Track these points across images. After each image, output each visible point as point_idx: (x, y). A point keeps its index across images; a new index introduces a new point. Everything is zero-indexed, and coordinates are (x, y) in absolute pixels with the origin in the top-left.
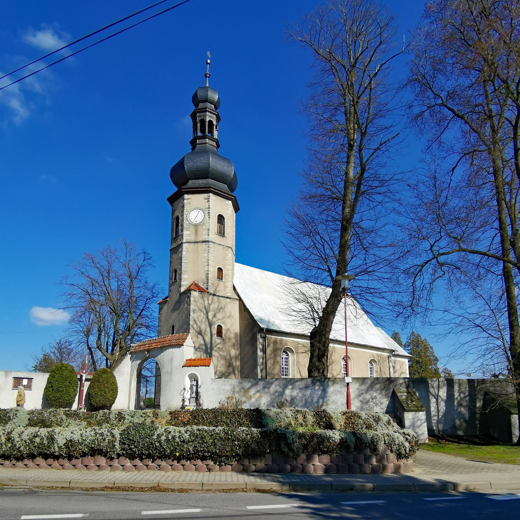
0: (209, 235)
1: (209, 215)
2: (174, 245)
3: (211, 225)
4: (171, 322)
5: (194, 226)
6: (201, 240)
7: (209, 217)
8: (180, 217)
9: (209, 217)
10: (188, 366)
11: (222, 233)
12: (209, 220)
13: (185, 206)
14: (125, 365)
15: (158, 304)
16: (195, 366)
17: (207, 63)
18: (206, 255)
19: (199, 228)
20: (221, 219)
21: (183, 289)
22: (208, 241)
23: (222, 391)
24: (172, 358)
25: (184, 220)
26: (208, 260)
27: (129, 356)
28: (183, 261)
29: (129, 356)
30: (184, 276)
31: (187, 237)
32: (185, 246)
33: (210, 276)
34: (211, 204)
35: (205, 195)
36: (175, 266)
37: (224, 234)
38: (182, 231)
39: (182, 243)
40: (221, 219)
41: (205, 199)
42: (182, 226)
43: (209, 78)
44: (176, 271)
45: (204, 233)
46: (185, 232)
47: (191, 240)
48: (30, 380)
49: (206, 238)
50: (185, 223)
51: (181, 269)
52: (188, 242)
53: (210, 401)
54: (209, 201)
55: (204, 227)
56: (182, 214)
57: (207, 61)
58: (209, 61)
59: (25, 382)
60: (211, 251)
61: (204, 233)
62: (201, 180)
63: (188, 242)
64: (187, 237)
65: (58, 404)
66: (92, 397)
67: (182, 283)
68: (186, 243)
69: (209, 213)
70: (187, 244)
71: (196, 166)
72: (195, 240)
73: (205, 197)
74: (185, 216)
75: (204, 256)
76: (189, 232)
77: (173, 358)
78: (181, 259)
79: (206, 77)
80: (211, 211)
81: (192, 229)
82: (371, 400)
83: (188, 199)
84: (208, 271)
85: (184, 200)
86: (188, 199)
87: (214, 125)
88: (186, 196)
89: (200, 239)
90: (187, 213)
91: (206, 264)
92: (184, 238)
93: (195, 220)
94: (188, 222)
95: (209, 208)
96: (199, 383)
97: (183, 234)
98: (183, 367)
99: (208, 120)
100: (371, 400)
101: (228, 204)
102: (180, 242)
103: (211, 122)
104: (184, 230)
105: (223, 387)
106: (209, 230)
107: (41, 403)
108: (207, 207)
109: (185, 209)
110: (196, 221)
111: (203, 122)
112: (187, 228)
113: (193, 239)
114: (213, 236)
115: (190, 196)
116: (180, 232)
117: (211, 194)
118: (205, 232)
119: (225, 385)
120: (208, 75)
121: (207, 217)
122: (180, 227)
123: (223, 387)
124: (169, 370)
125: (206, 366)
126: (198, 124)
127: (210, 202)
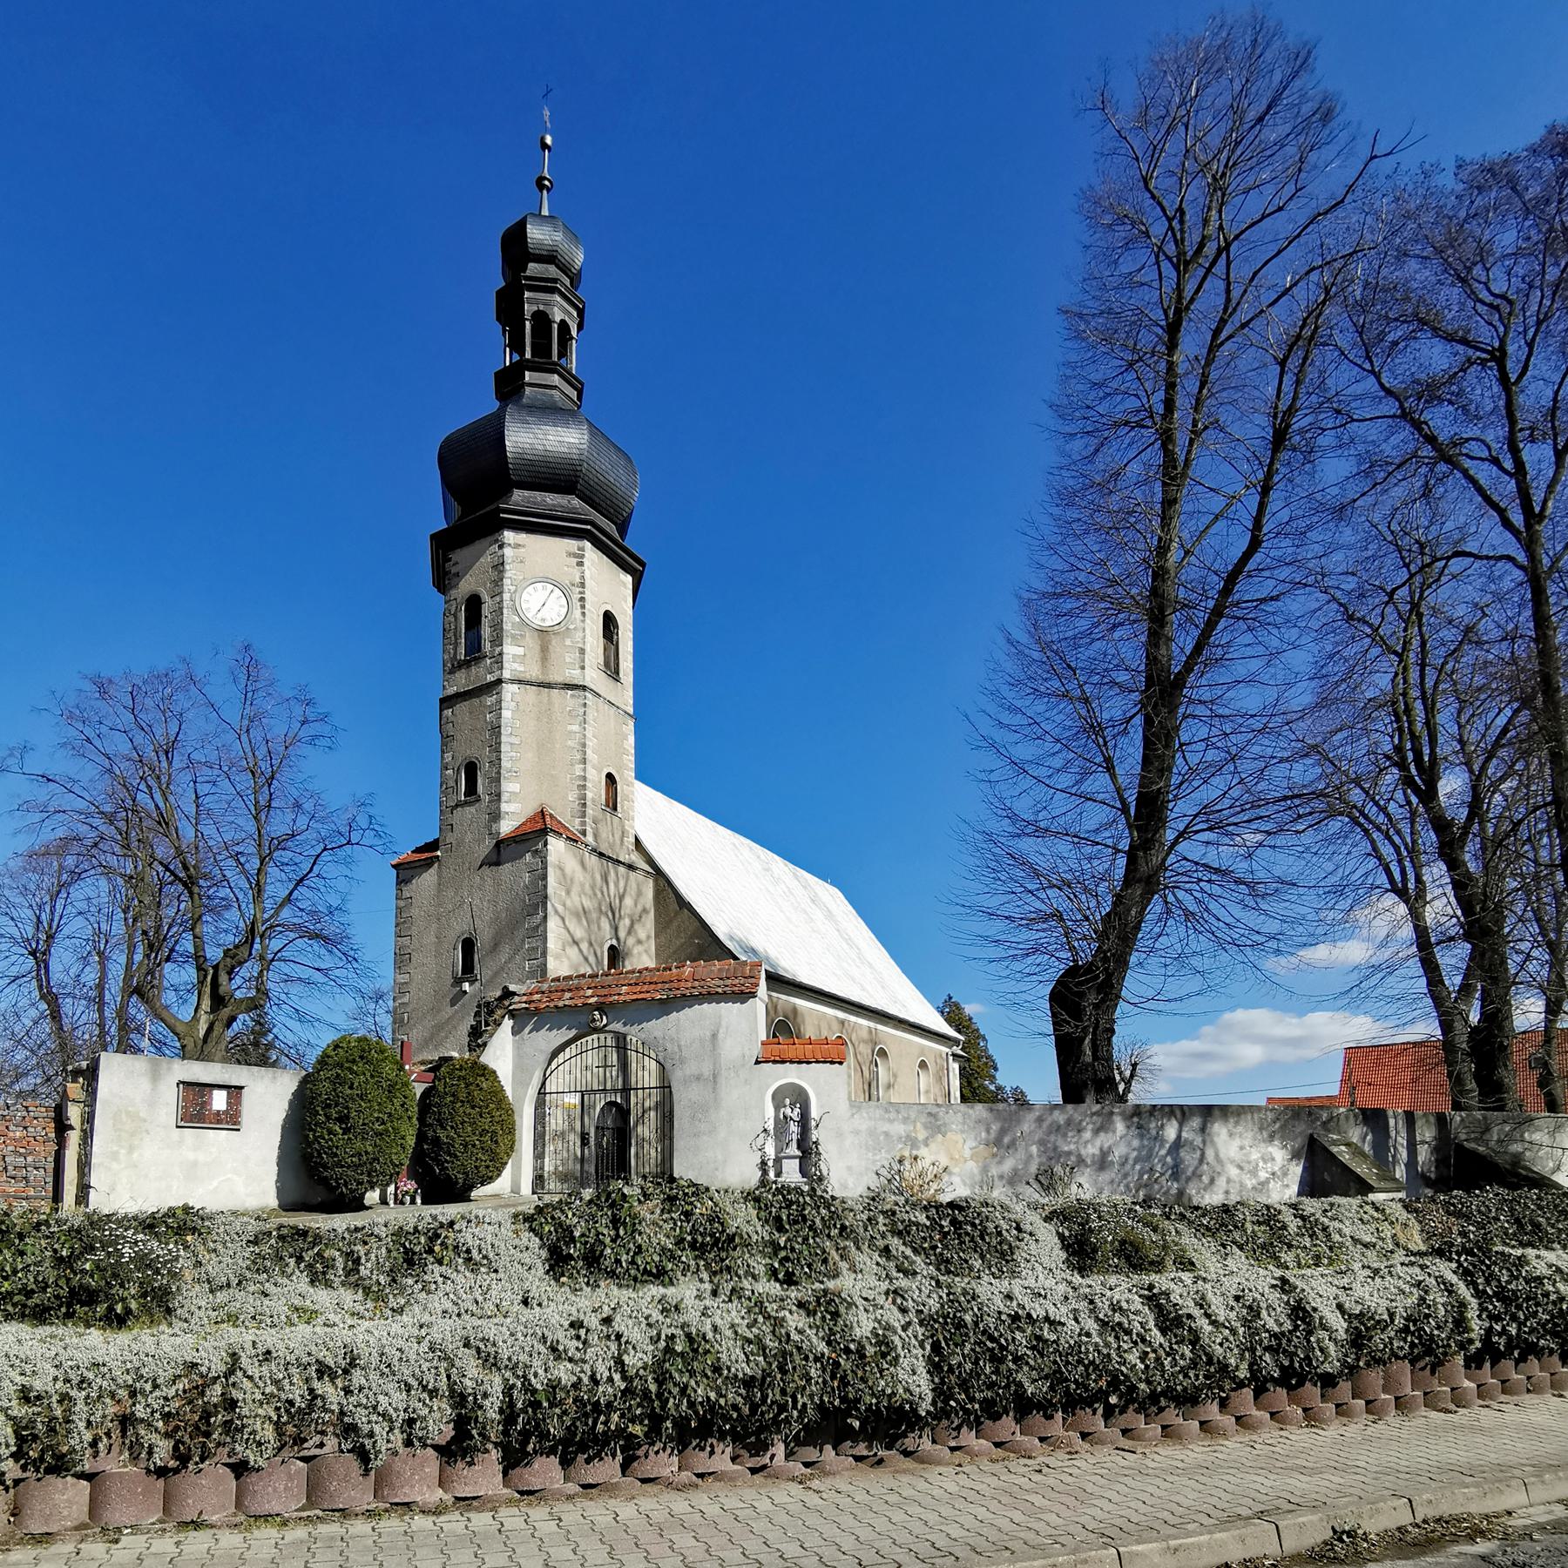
0: (583, 668)
1: (583, 607)
2: (461, 682)
3: (589, 639)
4: (459, 927)
5: (536, 633)
6: (559, 679)
7: (583, 614)
8: (485, 597)
9: (583, 614)
10: (775, 1062)
11: (612, 668)
12: (583, 621)
13: (507, 567)
14: (498, 1053)
15: (393, 866)
16: (800, 1062)
17: (544, 146)
18: (575, 728)
19: (553, 642)
20: (609, 621)
21: (506, 827)
22: (584, 688)
23: (882, 1138)
24: (714, 1036)
25: (505, 611)
26: (584, 745)
27: (508, 1023)
28: (503, 739)
29: (508, 1023)
30: (509, 787)
31: (516, 666)
32: (509, 691)
33: (589, 795)
34: (587, 575)
35: (571, 544)
36: (465, 749)
37: (617, 673)
38: (498, 640)
39: (499, 681)
40: (609, 621)
41: (570, 554)
42: (498, 627)
43: (549, 190)
44: (471, 769)
45: (568, 660)
46: (510, 649)
47: (527, 677)
48: (235, 1091)
49: (574, 675)
50: (509, 620)
51: (497, 762)
52: (520, 682)
53: (849, 1168)
54: (580, 564)
55: (568, 642)
56: (497, 590)
57: (543, 139)
58: (549, 140)
59: (219, 1101)
60: (590, 718)
61: (568, 660)
62: (552, 496)
63: (520, 682)
64: (516, 666)
65: (366, 1179)
66: (450, 1154)
67: (504, 807)
68: (513, 681)
69: (582, 599)
70: (516, 686)
71: (540, 447)
72: (541, 678)
73: (572, 550)
74: (506, 596)
75: (571, 732)
76: (520, 651)
77: (721, 1035)
78: (496, 730)
79: (541, 187)
80: (588, 595)
81: (531, 641)
82: (1261, 1164)
83: (517, 546)
84: (585, 778)
85: (501, 547)
86: (517, 546)
87: (572, 338)
88: (509, 536)
89: (557, 678)
90: (513, 588)
91: (578, 756)
92: (506, 665)
93: (539, 616)
94: (518, 619)
95: (583, 585)
96: (814, 1113)
97: (501, 654)
98: (757, 1062)
99: (558, 319)
100: (1261, 1164)
101: (624, 584)
102: (490, 678)
103: (563, 325)
104: (507, 641)
105: (886, 1127)
106: (582, 651)
107: (275, 1178)
108: (578, 580)
109: (507, 574)
110: (543, 620)
111: (542, 319)
112: (513, 637)
113: (534, 672)
114: (593, 676)
115: (522, 537)
116: (488, 645)
117: (588, 545)
118: (571, 657)
119: (891, 1121)
120: (547, 183)
121: (577, 613)
122: (486, 631)
123: (886, 1127)
124: (706, 1072)
125: (832, 1063)
126: (527, 323)
127: (585, 567)
